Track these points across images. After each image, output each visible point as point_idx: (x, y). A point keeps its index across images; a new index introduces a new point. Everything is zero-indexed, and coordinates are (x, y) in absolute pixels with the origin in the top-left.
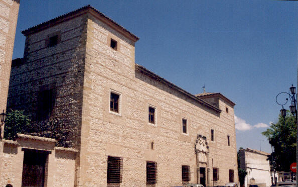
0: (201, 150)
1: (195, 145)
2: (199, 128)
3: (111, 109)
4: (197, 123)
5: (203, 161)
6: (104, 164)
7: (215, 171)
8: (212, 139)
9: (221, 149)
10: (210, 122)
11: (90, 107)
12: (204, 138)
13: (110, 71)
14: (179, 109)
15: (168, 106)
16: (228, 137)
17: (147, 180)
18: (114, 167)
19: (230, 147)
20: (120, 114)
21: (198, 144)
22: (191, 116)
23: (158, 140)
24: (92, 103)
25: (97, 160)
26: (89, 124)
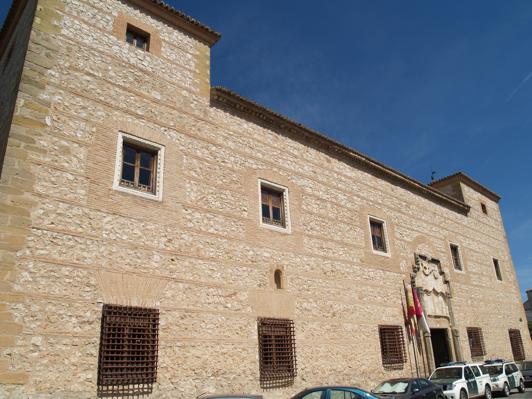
0: (431, 289)
1: (413, 278)
2: (420, 240)
3: (376, 248)
4: (413, 230)
5: (439, 313)
6: (87, 327)
7: (475, 336)
8: (458, 266)
9: (481, 286)
10: (447, 229)
11: (36, 170)
12: (435, 261)
13: (121, 91)
14: (358, 196)
15: (323, 188)
16: (496, 262)
17: (263, 369)
18: (128, 343)
19: (503, 282)
20: (159, 196)
21: (420, 274)
22: (392, 214)
23: (289, 264)
24: (47, 159)
25: (53, 318)
26: (29, 215)
